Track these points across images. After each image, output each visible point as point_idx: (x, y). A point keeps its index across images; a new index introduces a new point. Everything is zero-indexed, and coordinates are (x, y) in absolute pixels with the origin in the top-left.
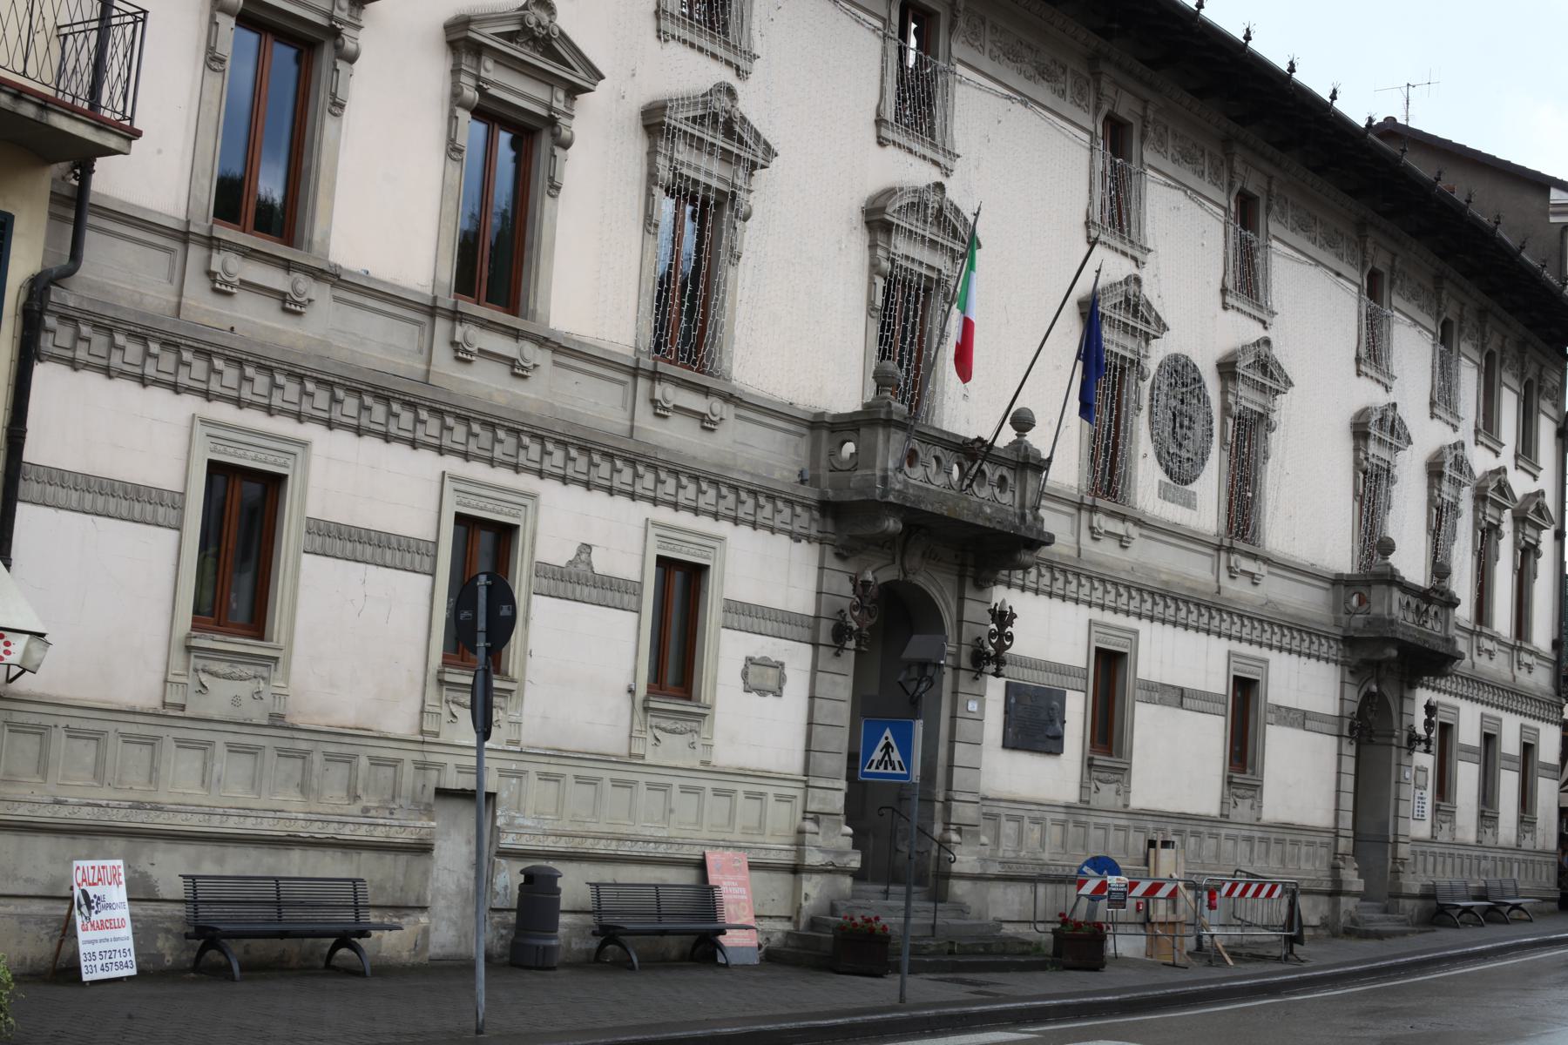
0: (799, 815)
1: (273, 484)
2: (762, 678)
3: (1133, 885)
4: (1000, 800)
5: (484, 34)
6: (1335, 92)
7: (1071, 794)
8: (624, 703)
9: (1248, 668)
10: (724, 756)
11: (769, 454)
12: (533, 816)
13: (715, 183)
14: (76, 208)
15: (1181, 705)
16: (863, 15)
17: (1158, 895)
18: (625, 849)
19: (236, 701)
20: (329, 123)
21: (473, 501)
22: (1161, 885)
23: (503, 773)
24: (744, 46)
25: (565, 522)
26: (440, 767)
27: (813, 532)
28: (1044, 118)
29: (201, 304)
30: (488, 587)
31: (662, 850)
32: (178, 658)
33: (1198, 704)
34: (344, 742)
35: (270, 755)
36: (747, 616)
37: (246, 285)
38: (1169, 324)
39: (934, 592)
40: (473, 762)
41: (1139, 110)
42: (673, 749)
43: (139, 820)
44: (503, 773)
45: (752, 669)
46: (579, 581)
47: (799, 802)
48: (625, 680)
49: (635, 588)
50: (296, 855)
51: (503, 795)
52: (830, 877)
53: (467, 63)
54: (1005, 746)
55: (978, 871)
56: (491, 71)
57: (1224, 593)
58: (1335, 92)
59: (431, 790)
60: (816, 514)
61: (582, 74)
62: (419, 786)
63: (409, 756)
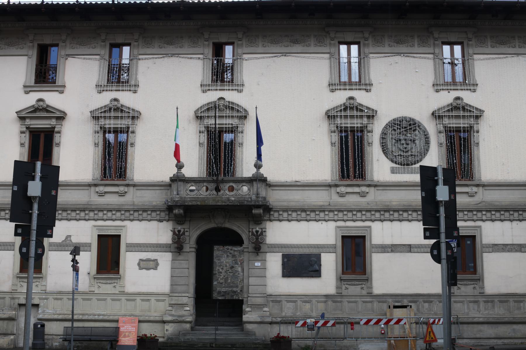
3: (316, 323)
4: (280, 295)
9: (470, 231)
10: (130, 288)
11: (155, 198)
13: (466, 126)
15: (410, 251)
16: (415, 55)
17: (328, 325)
20: (476, 148)
22: (328, 322)
23: (40, 299)
24: (368, 82)
26: (19, 298)
27: (167, 218)
28: (313, 58)
29: (336, 199)
31: (101, 317)
33: (416, 250)
35: (482, 305)
38: (482, 109)
39: (235, 228)
40: (71, 297)
42: (107, 288)
44: (40, 299)
45: (142, 263)
51: (41, 304)
52: (178, 324)
56: (446, 121)
59: (16, 304)
61: (58, 113)
62: (12, 304)
63: (7, 297)
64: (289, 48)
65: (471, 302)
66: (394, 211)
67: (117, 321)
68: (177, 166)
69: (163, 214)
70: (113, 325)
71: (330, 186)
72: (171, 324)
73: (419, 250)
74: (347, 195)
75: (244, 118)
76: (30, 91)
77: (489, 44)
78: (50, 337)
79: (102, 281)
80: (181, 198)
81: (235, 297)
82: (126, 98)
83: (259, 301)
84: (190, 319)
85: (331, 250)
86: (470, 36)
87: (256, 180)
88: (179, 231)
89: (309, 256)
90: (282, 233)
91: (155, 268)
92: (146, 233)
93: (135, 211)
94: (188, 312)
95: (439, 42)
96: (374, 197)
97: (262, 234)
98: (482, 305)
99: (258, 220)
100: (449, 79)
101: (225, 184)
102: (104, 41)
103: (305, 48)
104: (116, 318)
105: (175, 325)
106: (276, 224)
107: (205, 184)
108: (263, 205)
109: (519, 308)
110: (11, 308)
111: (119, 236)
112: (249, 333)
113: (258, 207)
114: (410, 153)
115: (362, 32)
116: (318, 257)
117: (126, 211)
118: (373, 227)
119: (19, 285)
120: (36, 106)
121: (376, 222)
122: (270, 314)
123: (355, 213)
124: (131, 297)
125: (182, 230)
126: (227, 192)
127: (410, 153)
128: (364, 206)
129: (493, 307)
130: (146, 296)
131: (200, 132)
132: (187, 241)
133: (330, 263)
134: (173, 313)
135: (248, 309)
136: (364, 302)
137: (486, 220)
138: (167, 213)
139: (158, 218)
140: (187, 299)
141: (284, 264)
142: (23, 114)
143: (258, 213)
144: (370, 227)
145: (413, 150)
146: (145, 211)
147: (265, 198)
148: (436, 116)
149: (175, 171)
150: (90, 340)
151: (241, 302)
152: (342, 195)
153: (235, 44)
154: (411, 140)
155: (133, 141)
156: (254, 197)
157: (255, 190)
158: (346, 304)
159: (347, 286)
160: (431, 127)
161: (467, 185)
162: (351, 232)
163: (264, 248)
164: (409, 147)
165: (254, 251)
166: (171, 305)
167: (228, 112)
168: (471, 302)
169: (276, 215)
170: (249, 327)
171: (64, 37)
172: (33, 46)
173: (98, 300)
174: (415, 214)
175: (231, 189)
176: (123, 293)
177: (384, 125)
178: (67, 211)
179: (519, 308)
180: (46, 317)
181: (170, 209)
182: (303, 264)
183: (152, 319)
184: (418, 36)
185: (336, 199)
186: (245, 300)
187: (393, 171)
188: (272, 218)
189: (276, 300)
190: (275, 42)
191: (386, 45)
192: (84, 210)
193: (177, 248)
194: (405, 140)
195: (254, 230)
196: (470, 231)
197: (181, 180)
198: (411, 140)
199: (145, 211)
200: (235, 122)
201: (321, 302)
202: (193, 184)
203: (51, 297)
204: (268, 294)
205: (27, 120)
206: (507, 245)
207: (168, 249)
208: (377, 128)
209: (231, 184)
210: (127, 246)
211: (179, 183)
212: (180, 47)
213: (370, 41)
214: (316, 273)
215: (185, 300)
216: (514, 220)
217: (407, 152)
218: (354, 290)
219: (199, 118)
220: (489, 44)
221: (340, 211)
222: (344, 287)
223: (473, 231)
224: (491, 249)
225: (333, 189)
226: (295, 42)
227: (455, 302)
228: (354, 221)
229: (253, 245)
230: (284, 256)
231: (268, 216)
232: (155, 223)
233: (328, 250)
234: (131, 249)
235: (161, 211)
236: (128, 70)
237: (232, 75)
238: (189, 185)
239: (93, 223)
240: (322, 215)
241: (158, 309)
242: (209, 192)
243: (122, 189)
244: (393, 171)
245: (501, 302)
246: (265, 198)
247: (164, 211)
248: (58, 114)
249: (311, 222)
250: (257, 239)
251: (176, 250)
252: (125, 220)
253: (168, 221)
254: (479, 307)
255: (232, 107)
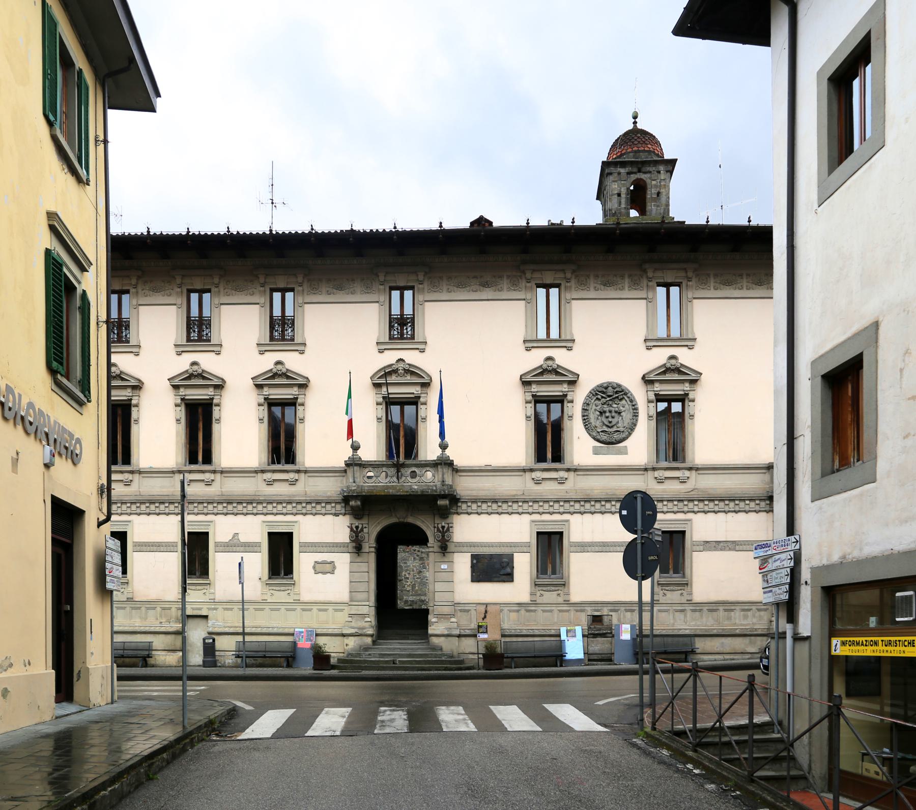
5: (652, 377)
7: (525, 598)
12: (221, 620)
25: (221, 528)
27: (343, 511)
30: (642, 544)
34: (151, 604)
36: (309, 547)
42: (281, 596)
46: (234, 545)
48: (258, 575)
49: (258, 545)
53: (650, 387)
55: (446, 632)
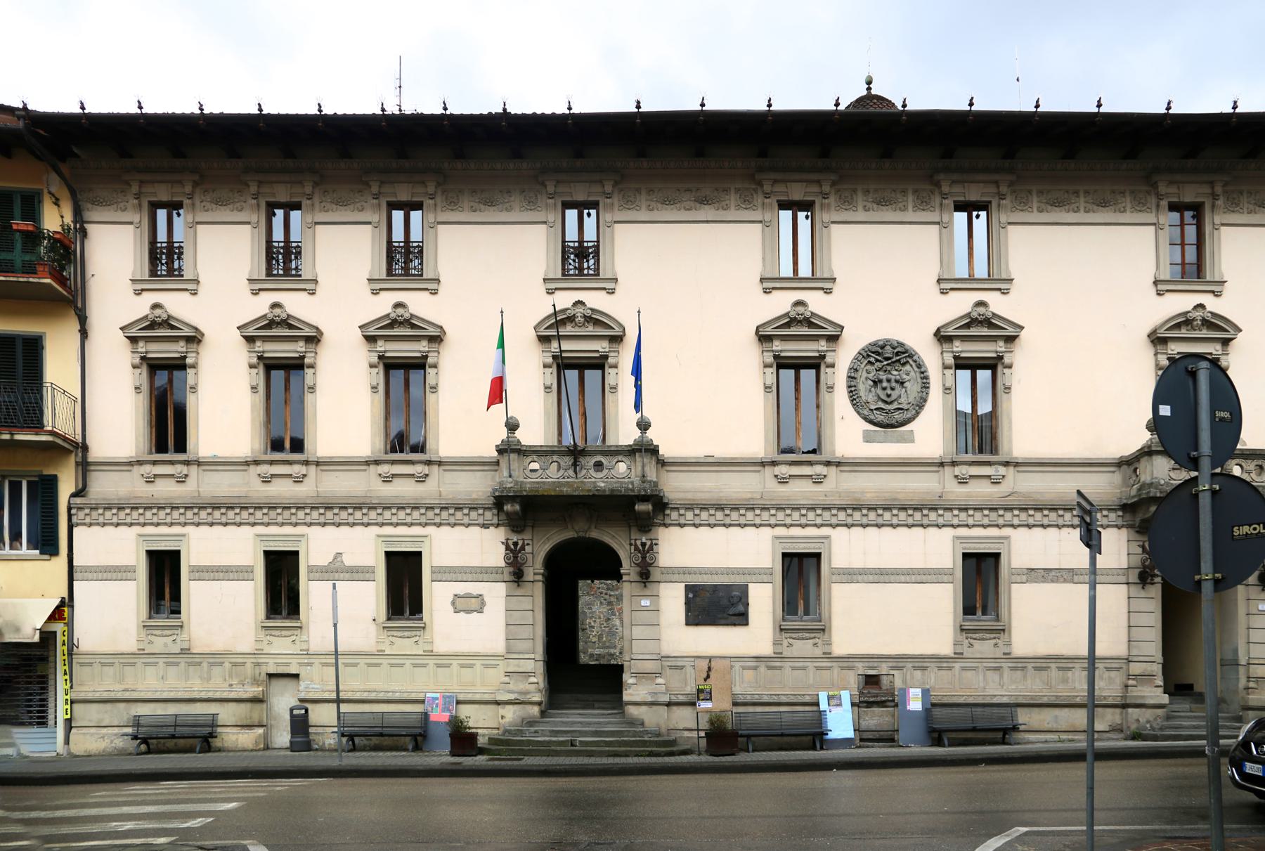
0: (1124, 678)
1: (175, 555)
2: (469, 605)
6: (638, 102)
8: (373, 628)
10: (441, 646)
11: (478, 486)
14: (85, 467)
18: (373, 696)
19: (166, 645)
21: (271, 544)
27: (495, 521)
32: (143, 633)
34: (215, 658)
35: (1006, 673)
37: (971, 477)
39: (607, 539)
41: (1209, 191)
43: (127, 695)
44: (300, 664)
46: (336, 571)
47: (1123, 672)
50: (198, 705)
54: (687, 624)
57: (444, 494)
58: (638, 102)
59: (264, 674)
60: (1120, 513)
63: (249, 661)
64: (210, 213)
65: (989, 669)
66: (869, 509)
67: (423, 702)
68: (639, 425)
69: (488, 515)
70: (418, 708)
71: (763, 464)
72: (508, 707)
73: (908, 578)
74: (791, 481)
75: (617, 339)
76: (952, 289)
77: (1035, 205)
78: (320, 730)
79: (395, 633)
80: (516, 483)
81: (613, 662)
82: (419, 304)
83: (650, 666)
84: (537, 697)
85: (765, 578)
86: (1004, 189)
87: (640, 450)
88: (515, 544)
89: (728, 588)
90: (686, 549)
91: (480, 610)
92: (465, 551)
93: (442, 509)
94: (535, 684)
95: (773, 201)
96: (839, 485)
97: (651, 548)
98: (1006, 673)
99: (645, 524)
100: (787, 271)
101: (588, 458)
102: (551, 196)
103: (721, 212)
104: (421, 697)
105: (516, 707)
106: (675, 530)
107: (555, 458)
108: (652, 496)
109: (1065, 681)
110: (255, 681)
111: (420, 554)
112: (633, 722)
113: (645, 499)
114: (895, 406)
115: (601, 182)
116: (744, 590)
117: (427, 508)
118: (1013, 539)
119: (265, 642)
120: (270, 316)
121: (839, 529)
122: (667, 690)
123: (804, 512)
124: (444, 660)
125: (520, 543)
126: (592, 472)
127: (895, 406)
128: (821, 500)
129: (1025, 677)
130: (467, 660)
131: (545, 366)
132: (530, 562)
133: (764, 601)
134: (511, 687)
135: (631, 681)
136: (818, 668)
137: (1019, 526)
138: (495, 511)
139: (481, 521)
140: (533, 663)
141: (688, 603)
142: (372, 332)
143: (643, 510)
144: (827, 537)
145: (902, 400)
146: (458, 508)
147: (656, 484)
148: (942, 337)
149: (503, 433)
150: (381, 735)
151: (620, 669)
152: (962, 481)
153: (994, 205)
154: (897, 381)
155: (830, 383)
156: (637, 481)
157: (639, 468)
158: (787, 671)
159: (791, 641)
160: (931, 357)
161: (989, 463)
162: (796, 546)
163: (655, 575)
164: (895, 394)
165: (638, 579)
166: (508, 674)
167: (591, 329)
168: (989, 669)
169: (674, 515)
170: (632, 710)
171: (431, 189)
172: (258, 205)
173: (392, 665)
174: (1068, 516)
175: (599, 466)
176: (430, 654)
177: (854, 353)
178: (219, 508)
179: (1065, 681)
180: (312, 696)
181: (499, 502)
182: (716, 604)
183: (477, 697)
184: (915, 191)
185: (772, 485)
186: (626, 664)
187: (868, 438)
188: (668, 521)
189: (672, 663)
190: (668, 202)
191: (860, 208)
192: (358, 507)
193: (514, 574)
194: (889, 381)
195: (639, 543)
196: (992, 546)
197: (514, 451)
198: (897, 381)
199: (458, 508)
200: (601, 346)
201: (749, 668)
202: (535, 458)
203: (317, 661)
204: (663, 654)
205: (776, 343)
206: (1051, 570)
207: (498, 577)
208: (844, 357)
209: (599, 458)
210: (433, 572)
211: (512, 456)
212: (507, 210)
213: (615, 200)
214: (741, 618)
215: (529, 666)
216: (1064, 526)
217: (891, 403)
218: (803, 647)
219: (764, 338)
220: (1035, 205)
221: (779, 509)
222: (785, 643)
223: (997, 546)
224: (1024, 578)
225: (768, 469)
226: (704, 201)
227: (346, 665)
228: (803, 526)
229: (638, 569)
230: (689, 588)
231: (661, 517)
232: (476, 530)
233: (760, 578)
234: (439, 576)
235: (485, 509)
236: (421, 252)
237: (597, 262)
238: (530, 459)
239: (375, 530)
240: (933, 515)
241: (489, 682)
242: (562, 472)
243: (419, 469)
244: (868, 438)
245: (1036, 669)
246: (656, 484)
247: (489, 509)
248: (308, 332)
249: (731, 529)
250: (644, 558)
251: (512, 578)
252: (426, 524)
253: (498, 526)
254: (1001, 676)
255: (594, 319)
